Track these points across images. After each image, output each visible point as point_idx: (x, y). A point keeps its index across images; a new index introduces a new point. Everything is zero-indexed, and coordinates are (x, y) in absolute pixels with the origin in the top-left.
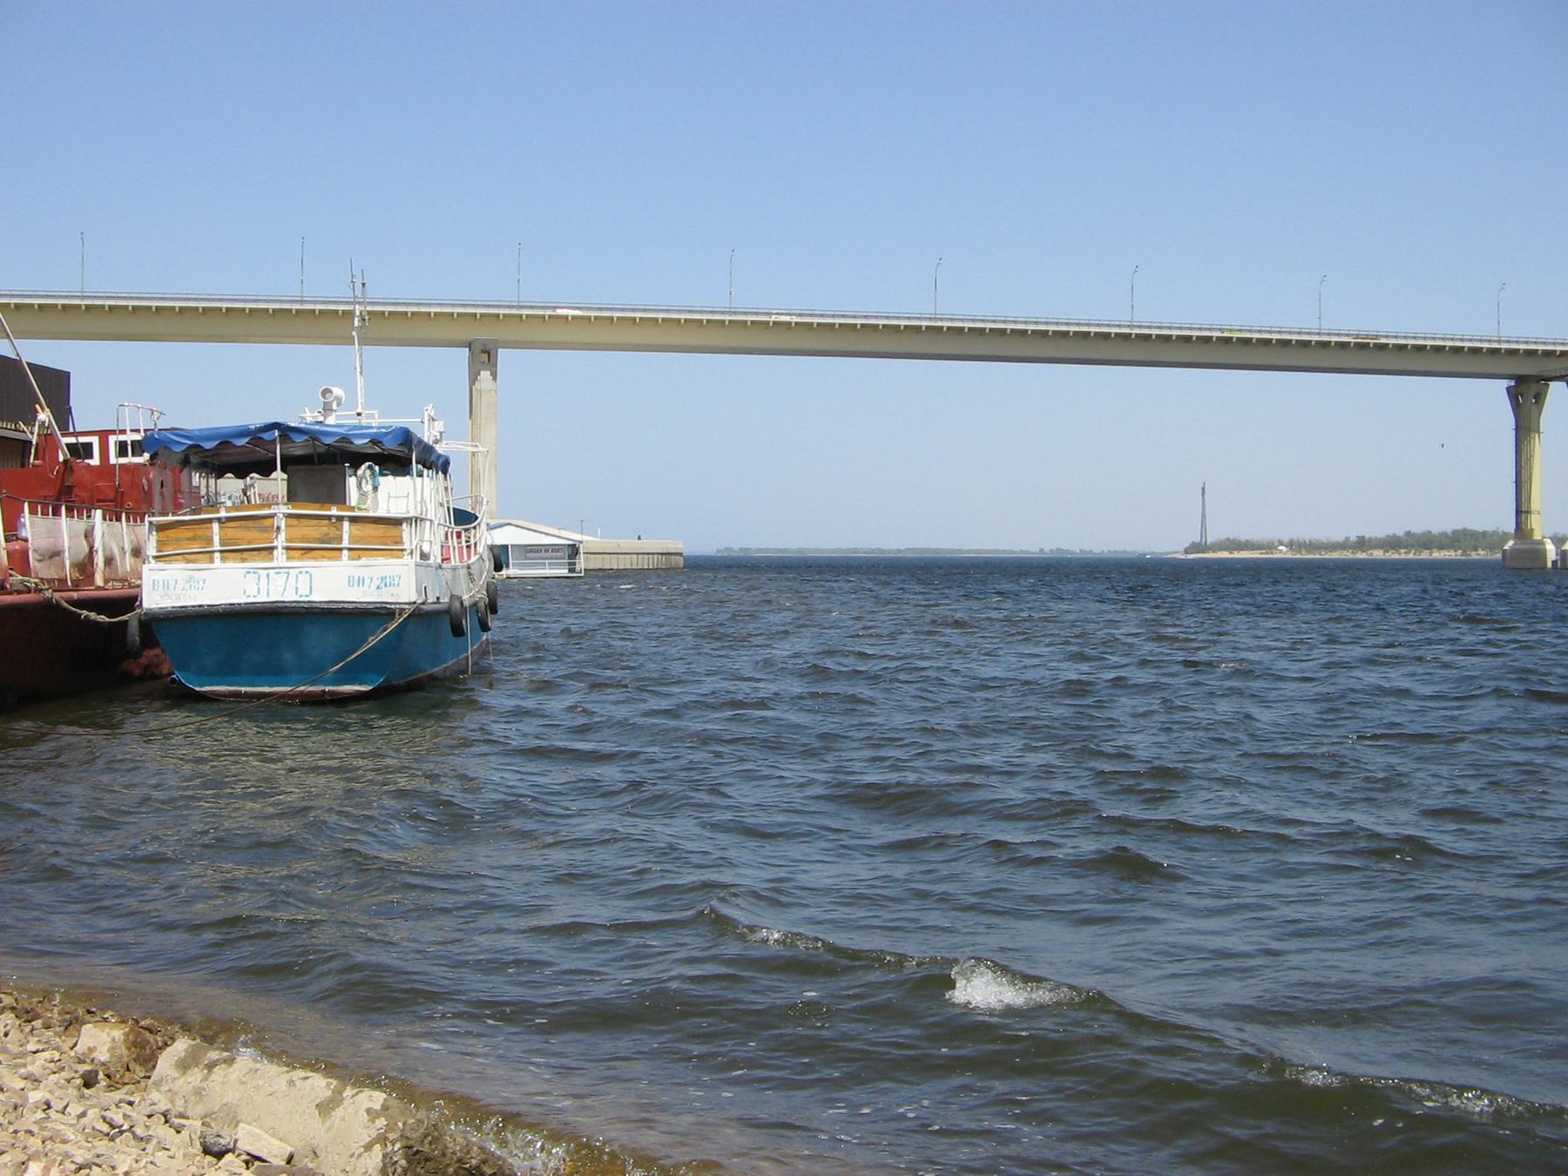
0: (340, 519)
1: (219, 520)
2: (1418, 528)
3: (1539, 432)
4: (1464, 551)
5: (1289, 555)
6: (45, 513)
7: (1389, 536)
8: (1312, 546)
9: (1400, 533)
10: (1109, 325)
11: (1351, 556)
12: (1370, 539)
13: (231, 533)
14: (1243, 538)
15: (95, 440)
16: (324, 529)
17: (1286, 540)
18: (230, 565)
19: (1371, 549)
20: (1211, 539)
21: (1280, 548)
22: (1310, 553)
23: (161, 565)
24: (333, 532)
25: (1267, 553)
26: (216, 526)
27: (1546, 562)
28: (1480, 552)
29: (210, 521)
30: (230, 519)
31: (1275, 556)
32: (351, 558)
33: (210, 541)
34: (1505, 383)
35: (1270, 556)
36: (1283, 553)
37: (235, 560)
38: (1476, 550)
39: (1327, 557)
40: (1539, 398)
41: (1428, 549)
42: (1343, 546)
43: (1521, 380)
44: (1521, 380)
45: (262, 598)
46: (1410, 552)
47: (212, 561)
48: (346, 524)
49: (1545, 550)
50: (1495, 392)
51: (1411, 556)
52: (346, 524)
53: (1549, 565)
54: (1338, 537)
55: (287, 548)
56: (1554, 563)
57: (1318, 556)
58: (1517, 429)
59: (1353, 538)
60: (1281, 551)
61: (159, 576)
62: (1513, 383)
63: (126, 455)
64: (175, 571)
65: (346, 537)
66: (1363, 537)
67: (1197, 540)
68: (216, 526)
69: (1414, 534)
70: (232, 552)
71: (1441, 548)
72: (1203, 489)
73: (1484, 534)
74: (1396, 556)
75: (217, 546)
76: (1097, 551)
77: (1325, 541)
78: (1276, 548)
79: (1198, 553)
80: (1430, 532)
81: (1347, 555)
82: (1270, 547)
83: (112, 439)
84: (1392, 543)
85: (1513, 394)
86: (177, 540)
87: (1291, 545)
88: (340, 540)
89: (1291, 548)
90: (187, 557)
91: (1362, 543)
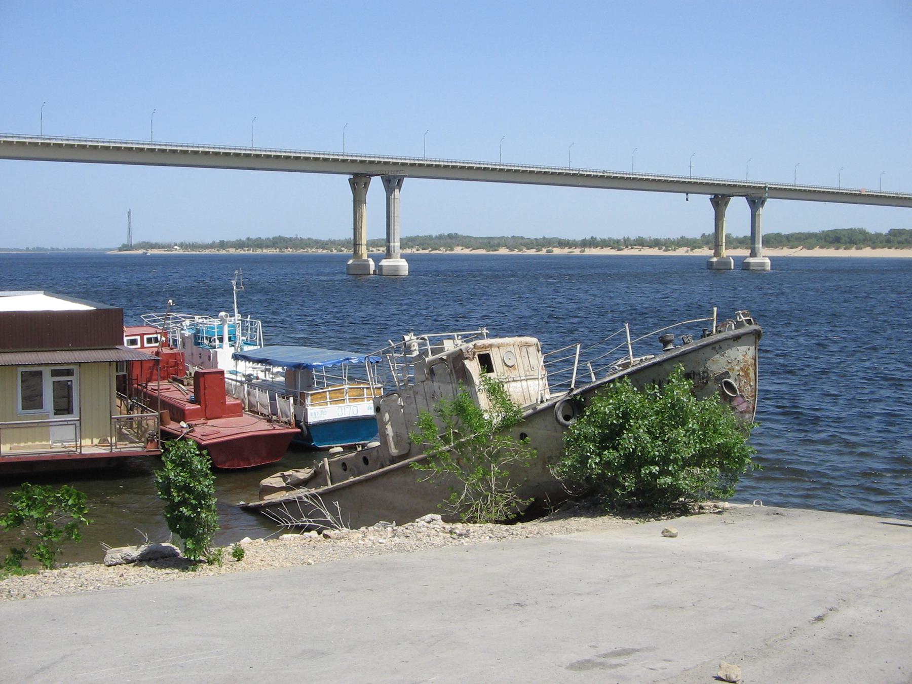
0: (363, 388)
1: (329, 391)
2: (254, 236)
3: (365, 203)
4: (281, 249)
5: (181, 252)
6: (262, 392)
7: (237, 240)
8: (194, 246)
9: (244, 238)
10: (143, 144)
11: (217, 252)
12: (227, 242)
13: (333, 395)
14: (153, 241)
15: (138, 338)
16: (358, 392)
17: (178, 242)
18: (333, 406)
19: (228, 248)
20: (135, 241)
21: (175, 247)
22: (193, 250)
23: (312, 408)
24: (361, 393)
25: (168, 251)
26: (328, 393)
27: (369, 271)
28: (289, 249)
29: (326, 392)
30: (332, 391)
31: (173, 252)
32: (368, 401)
33: (326, 398)
34: (348, 177)
35: (170, 253)
36: (178, 251)
37: (334, 404)
38: (287, 248)
39: (203, 253)
40: (366, 185)
41: (261, 248)
42: (212, 246)
43: (356, 175)
44: (356, 175)
45: (343, 416)
46: (250, 249)
47: (327, 405)
48: (365, 390)
49: (369, 265)
50: (343, 181)
51: (251, 252)
52: (365, 390)
53: (372, 272)
54: (209, 240)
55: (349, 399)
56: (375, 271)
57: (198, 253)
58: (354, 201)
59: (217, 241)
60: (176, 249)
61: (313, 411)
62: (352, 177)
63: (151, 343)
64: (317, 409)
65: (365, 394)
66: (223, 241)
67: (126, 243)
68: (328, 393)
69: (251, 239)
70: (334, 401)
71: (267, 247)
72: (129, 213)
73: (291, 239)
74: (242, 252)
75: (328, 400)
76: (61, 247)
77: (201, 243)
78: (173, 247)
79: (127, 250)
80: (260, 238)
81: (214, 252)
82: (169, 247)
83: (145, 337)
84: (240, 245)
85: (354, 184)
86: (317, 399)
87: (182, 245)
88: (364, 395)
89: (182, 248)
90: (320, 404)
91: (223, 245)
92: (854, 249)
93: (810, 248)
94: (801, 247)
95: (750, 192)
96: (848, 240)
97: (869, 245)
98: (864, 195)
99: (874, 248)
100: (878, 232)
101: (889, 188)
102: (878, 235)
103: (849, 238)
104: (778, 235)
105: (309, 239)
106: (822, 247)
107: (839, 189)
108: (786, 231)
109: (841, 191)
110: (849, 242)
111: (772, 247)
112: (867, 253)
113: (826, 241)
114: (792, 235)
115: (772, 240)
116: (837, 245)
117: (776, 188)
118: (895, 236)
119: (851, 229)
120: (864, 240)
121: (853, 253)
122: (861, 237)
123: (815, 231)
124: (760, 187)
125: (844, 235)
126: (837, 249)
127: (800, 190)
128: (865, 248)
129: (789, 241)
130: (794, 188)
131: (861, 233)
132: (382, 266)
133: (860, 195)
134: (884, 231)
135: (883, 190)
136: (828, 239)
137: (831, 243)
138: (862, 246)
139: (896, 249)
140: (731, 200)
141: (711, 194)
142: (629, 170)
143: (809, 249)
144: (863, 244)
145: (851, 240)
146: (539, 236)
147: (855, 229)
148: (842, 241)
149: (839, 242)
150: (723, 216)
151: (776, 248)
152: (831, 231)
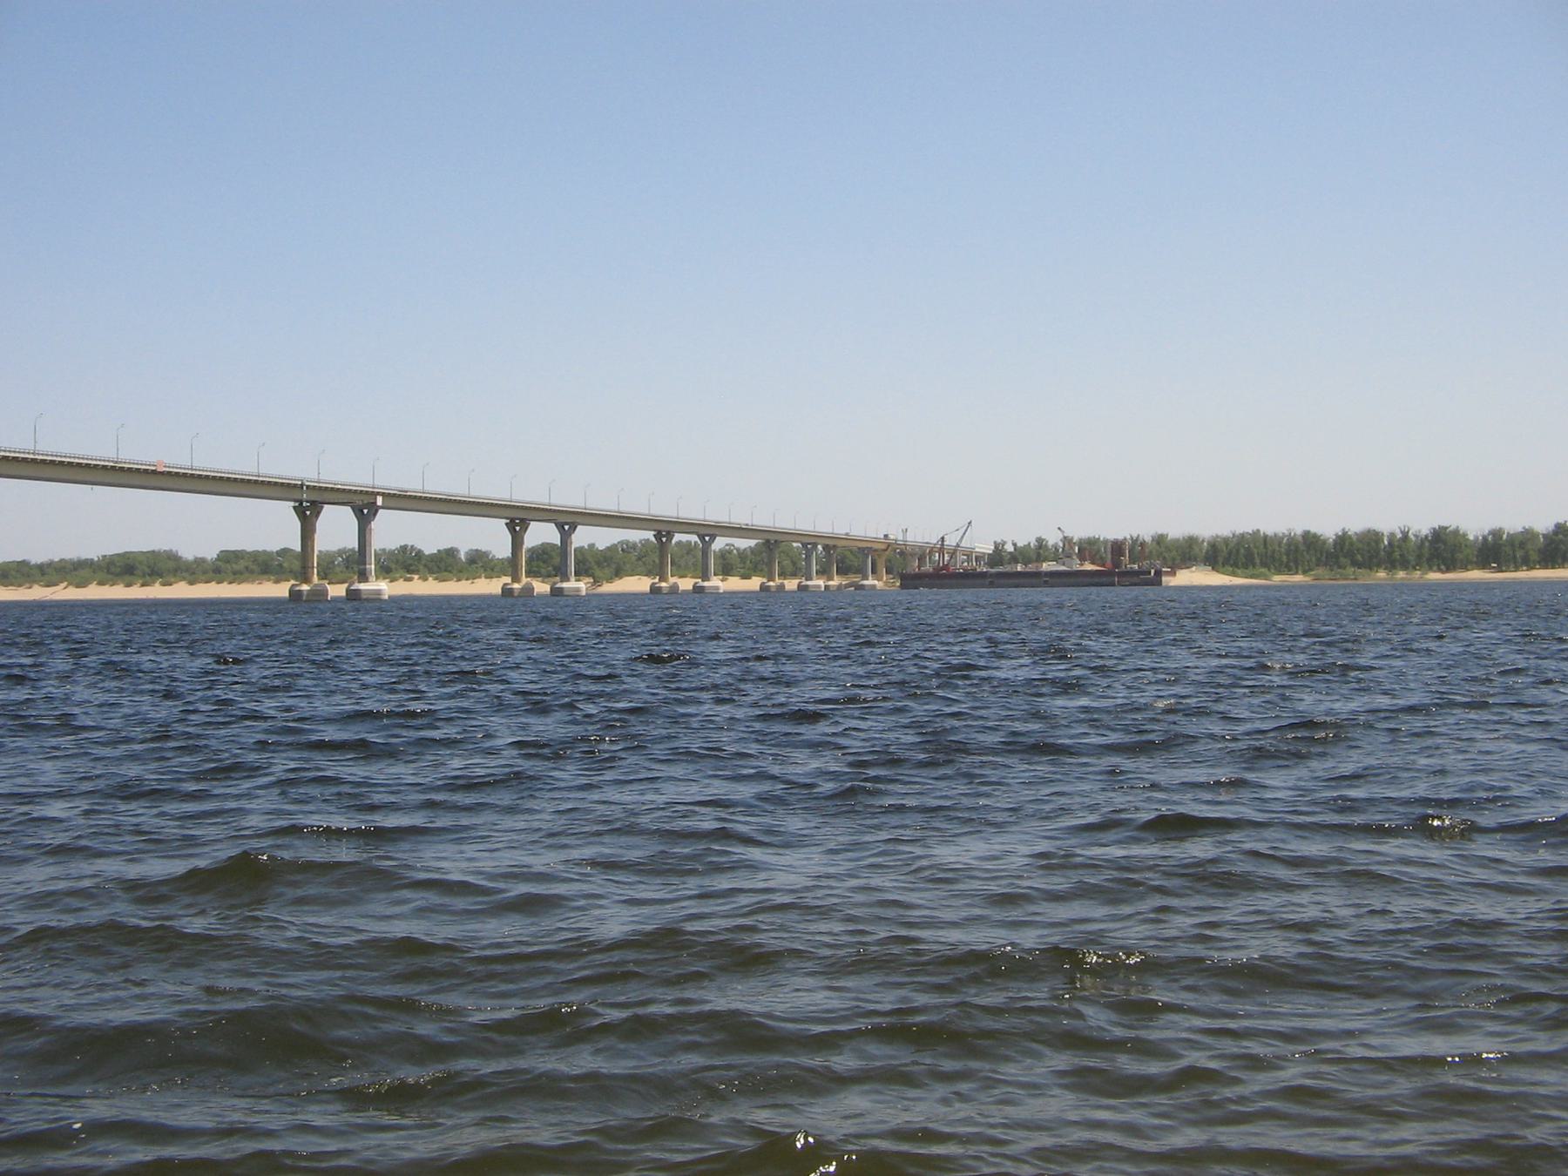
62: (297, 504)
92: (157, 585)
93: (81, 584)
94: (66, 583)
95: (355, 498)
96: (147, 570)
97: (184, 579)
98: (162, 473)
99: (191, 583)
100: (199, 556)
101: (438, 485)
102: (200, 562)
103: (149, 567)
104: (24, 563)
105: (61, 560)
106: (101, 583)
107: (259, 476)
108: (37, 558)
109: (261, 479)
110: (149, 575)
111: (12, 585)
112: (181, 591)
113: (108, 572)
114: (50, 564)
115: (13, 573)
116: (128, 578)
117: (208, 476)
118: (228, 562)
119: (154, 551)
120: (176, 571)
121: (157, 592)
122: (171, 564)
123: (89, 557)
124: (295, 485)
125: (140, 563)
126: (129, 585)
127: (43, 461)
128: (176, 582)
129: (43, 575)
130: (32, 456)
131: (169, 558)
132: (467, 559)
133: (154, 472)
134: (211, 554)
135: (553, 501)
136: (113, 570)
137: (117, 575)
138: (173, 580)
139: (230, 583)
140: (324, 510)
141: (507, 518)
142: (507, 497)
143: (78, 586)
144: (175, 576)
145: (153, 570)
146: (1421, 524)
147: (159, 551)
148: (138, 572)
149: (132, 574)
150: (313, 531)
151: (20, 586)
152: (118, 555)
